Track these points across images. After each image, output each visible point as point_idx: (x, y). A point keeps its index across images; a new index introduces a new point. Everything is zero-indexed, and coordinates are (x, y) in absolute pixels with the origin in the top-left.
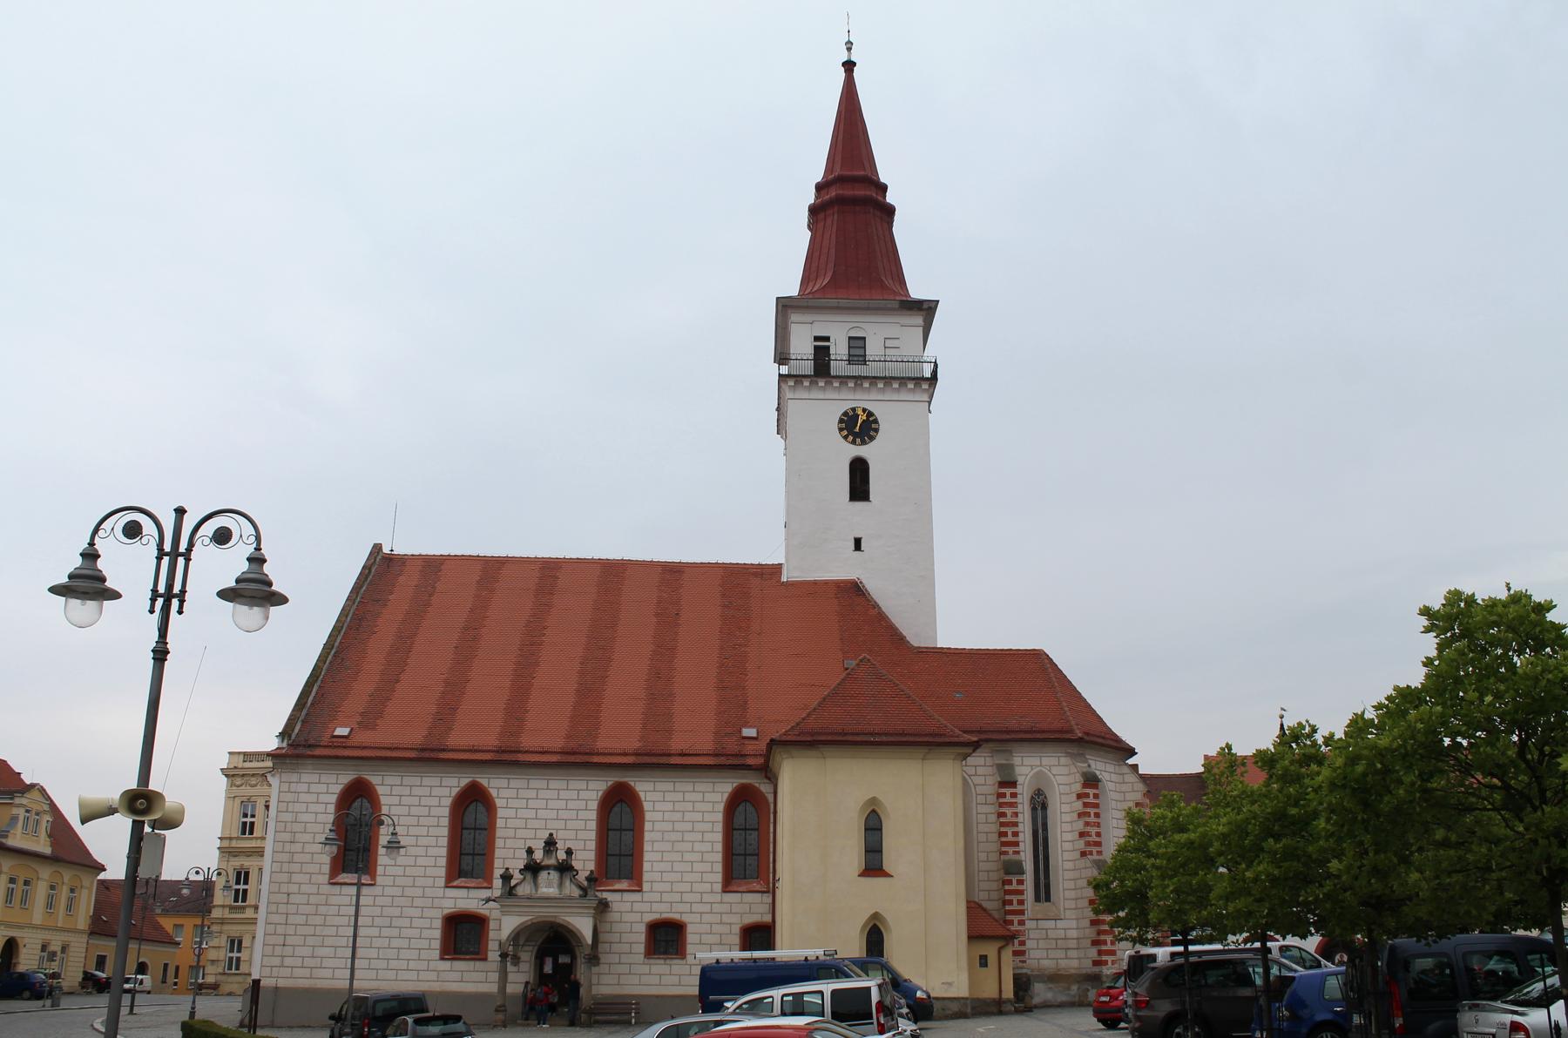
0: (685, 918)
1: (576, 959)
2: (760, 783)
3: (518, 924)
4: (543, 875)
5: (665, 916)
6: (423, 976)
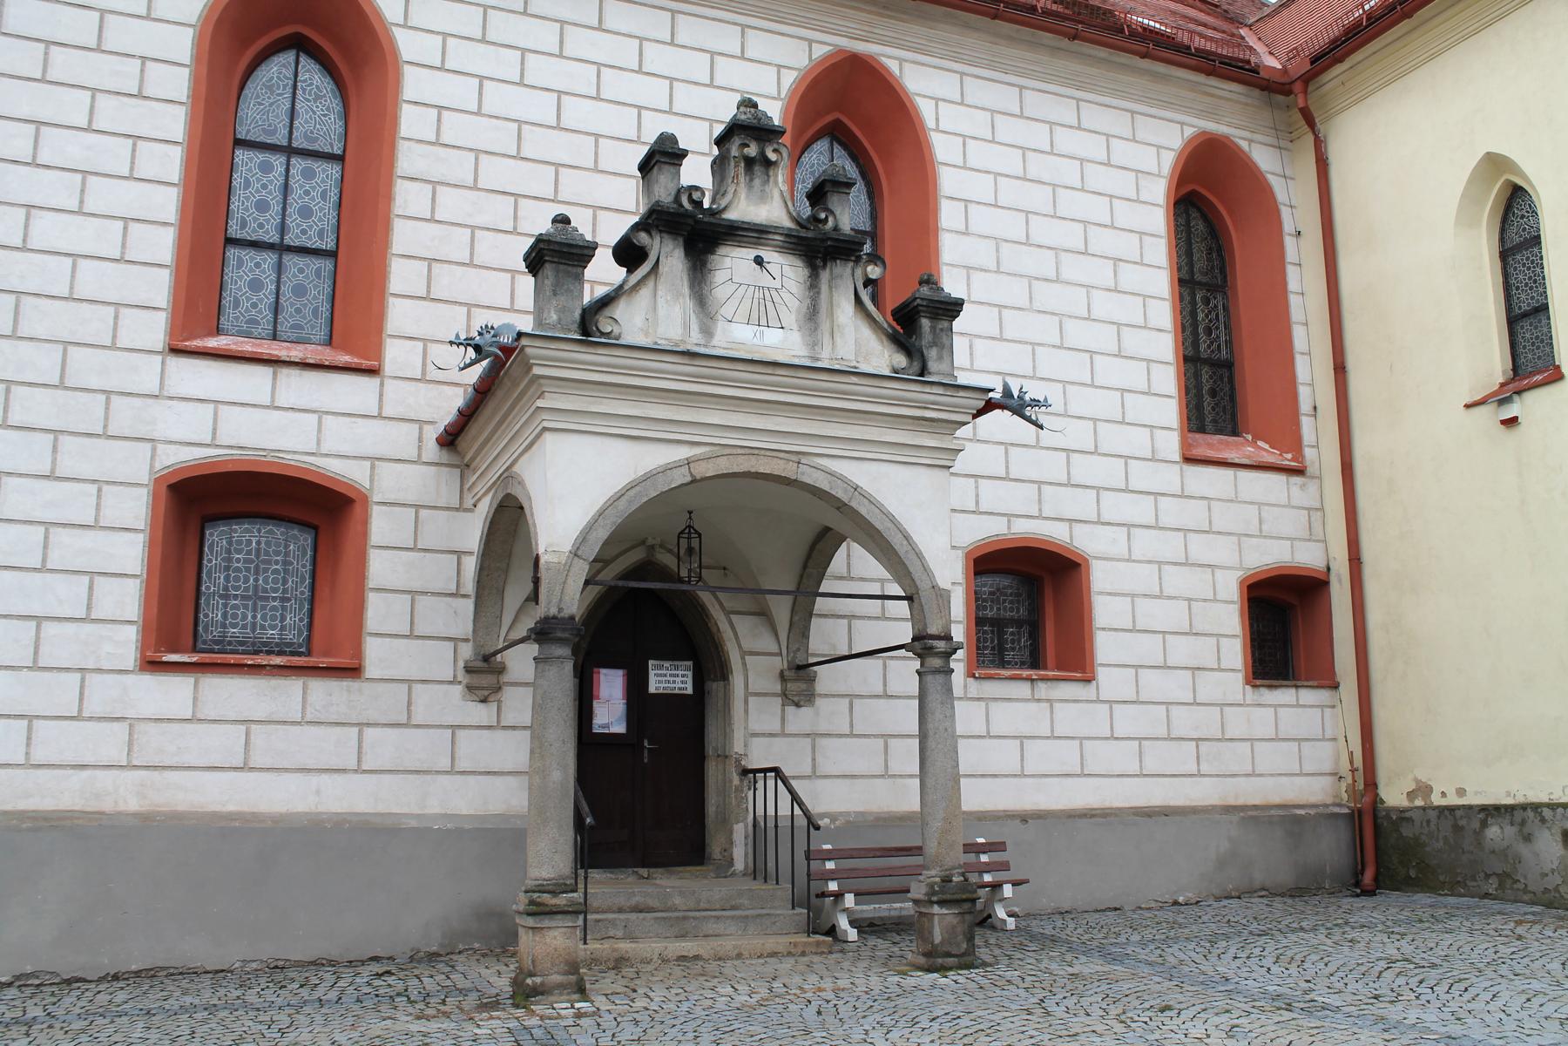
0: (1084, 541)
1: (723, 673)
2: (901, 61)
4: (733, 263)
6: (55, 741)
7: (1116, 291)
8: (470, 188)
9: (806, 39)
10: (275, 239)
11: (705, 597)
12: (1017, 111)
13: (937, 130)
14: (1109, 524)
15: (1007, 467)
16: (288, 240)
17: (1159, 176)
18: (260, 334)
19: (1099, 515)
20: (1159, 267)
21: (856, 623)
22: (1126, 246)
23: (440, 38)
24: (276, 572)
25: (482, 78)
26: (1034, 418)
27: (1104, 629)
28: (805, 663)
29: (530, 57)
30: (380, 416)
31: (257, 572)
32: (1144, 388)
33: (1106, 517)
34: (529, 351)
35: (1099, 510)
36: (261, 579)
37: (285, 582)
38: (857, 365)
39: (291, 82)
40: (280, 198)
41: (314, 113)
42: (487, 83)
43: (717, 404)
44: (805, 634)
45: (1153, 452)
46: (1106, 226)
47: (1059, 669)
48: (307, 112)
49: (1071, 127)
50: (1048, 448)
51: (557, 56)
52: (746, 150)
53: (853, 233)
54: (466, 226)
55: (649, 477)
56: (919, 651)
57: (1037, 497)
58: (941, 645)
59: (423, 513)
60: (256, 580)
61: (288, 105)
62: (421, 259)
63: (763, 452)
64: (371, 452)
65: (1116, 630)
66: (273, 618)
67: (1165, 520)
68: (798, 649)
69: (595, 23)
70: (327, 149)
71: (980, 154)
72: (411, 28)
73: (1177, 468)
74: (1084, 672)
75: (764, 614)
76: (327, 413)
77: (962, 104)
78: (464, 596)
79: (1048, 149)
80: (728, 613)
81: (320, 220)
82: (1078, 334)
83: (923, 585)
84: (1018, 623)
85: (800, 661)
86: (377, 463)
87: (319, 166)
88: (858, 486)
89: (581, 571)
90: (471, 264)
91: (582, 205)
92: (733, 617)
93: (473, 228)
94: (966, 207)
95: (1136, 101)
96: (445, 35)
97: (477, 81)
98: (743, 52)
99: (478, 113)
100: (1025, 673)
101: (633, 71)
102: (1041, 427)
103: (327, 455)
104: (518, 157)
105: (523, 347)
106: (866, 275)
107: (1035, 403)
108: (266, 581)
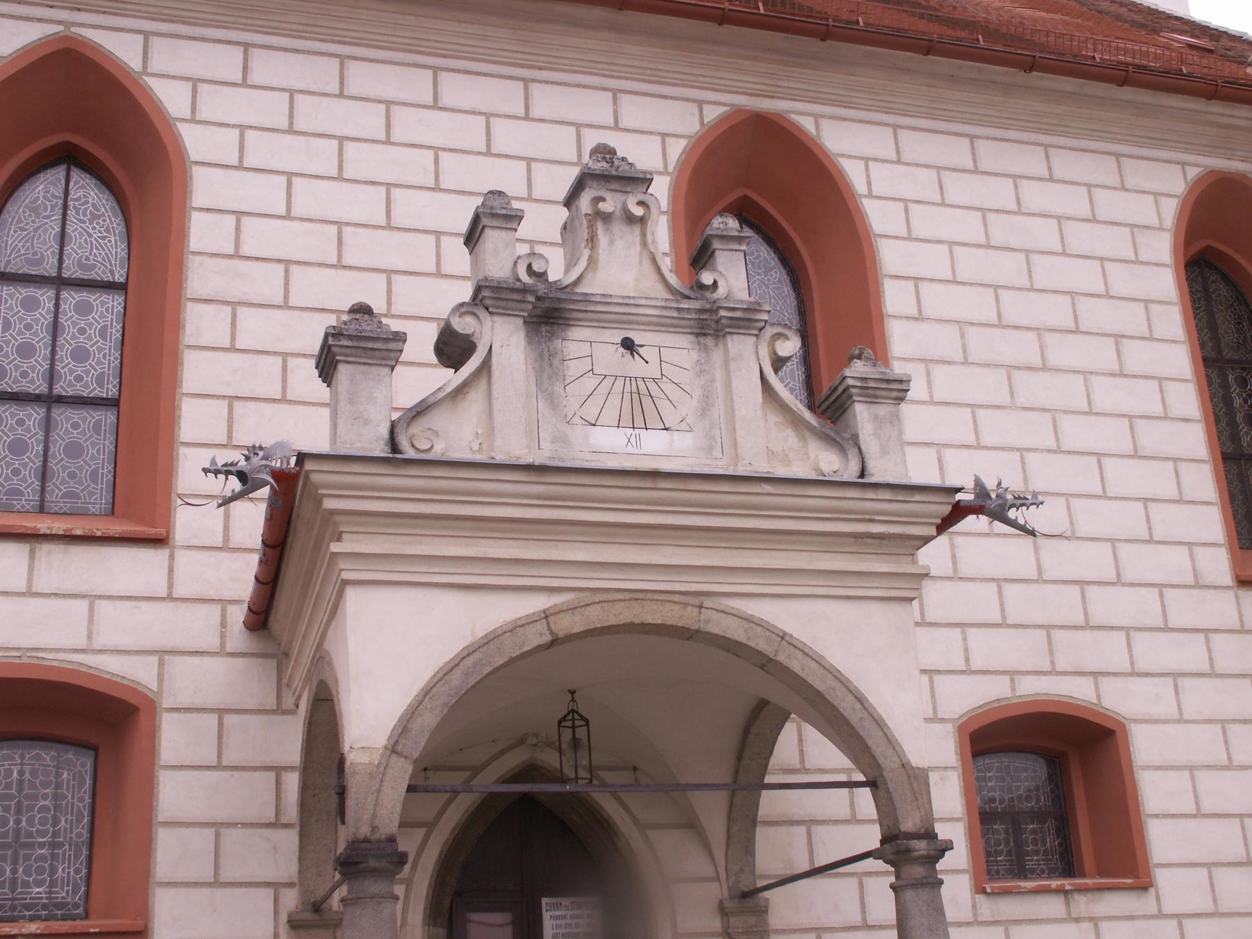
2: (817, 117)
3: (450, 649)
5: (1034, 688)
7: (1122, 375)
8: (279, 307)
9: (694, 101)
10: (43, 389)
11: (609, 806)
12: (970, 165)
13: (870, 195)
14: (1147, 675)
15: (1003, 610)
16: (58, 390)
17: (1161, 229)
18: (23, 506)
19: (1132, 663)
20: (1175, 342)
21: (818, 830)
22: (1129, 318)
23: (237, 132)
24: (44, 809)
25: (290, 175)
26: (1021, 521)
27: (1157, 816)
28: (752, 888)
29: (350, 147)
30: (170, 597)
31: (19, 811)
32: (1174, 494)
33: (1141, 666)
34: (315, 477)
35: (1131, 657)
36: (24, 819)
37: (56, 822)
38: (771, 470)
39: (61, 202)
40: (48, 339)
41: (90, 236)
42: (296, 180)
43: (581, 534)
44: (748, 849)
45: (1196, 576)
46: (1099, 296)
47: (1101, 874)
48: (81, 235)
49: (1040, 179)
50: (1055, 582)
51: (384, 143)
52: (601, 206)
53: (712, 250)
54: (275, 353)
55: (492, 638)
56: (891, 857)
57: (1046, 647)
58: (921, 846)
59: (229, 719)
60: (18, 822)
61: (57, 229)
62: (218, 397)
63: (649, 596)
64: (158, 643)
65: (1173, 816)
66: (40, 871)
67: (1222, 665)
68: (742, 871)
69: (430, 101)
70: (107, 277)
71: (926, 221)
72: (200, 122)
73: (1230, 595)
74: (1137, 877)
75: (692, 825)
76: (100, 597)
77: (899, 162)
78: (287, 826)
79: (1014, 207)
80: (642, 827)
81: (99, 362)
82: (1076, 432)
83: (889, 763)
84: (1039, 816)
85: (745, 886)
86: (166, 657)
87: (95, 298)
88: (785, 633)
89: (402, 772)
90: (284, 400)
91: (422, 318)
92: (651, 833)
93: (285, 356)
94: (916, 287)
95: (1120, 142)
96: (243, 128)
97: (284, 179)
98: (616, 121)
99: (287, 217)
100: (1055, 883)
101: (479, 153)
102: (1032, 533)
103: (101, 652)
104: (340, 266)
105: (308, 473)
106: (775, 353)
107: (1021, 502)
108: (31, 822)
